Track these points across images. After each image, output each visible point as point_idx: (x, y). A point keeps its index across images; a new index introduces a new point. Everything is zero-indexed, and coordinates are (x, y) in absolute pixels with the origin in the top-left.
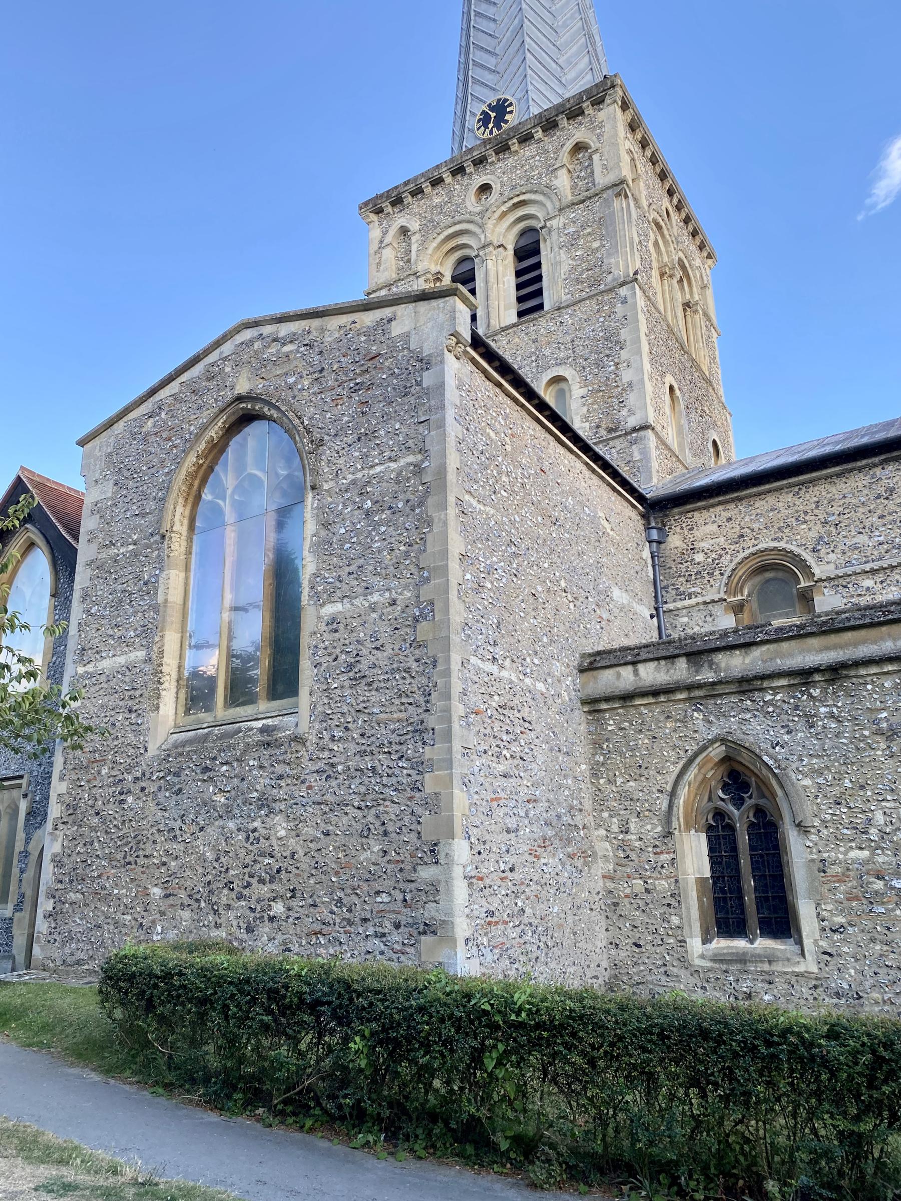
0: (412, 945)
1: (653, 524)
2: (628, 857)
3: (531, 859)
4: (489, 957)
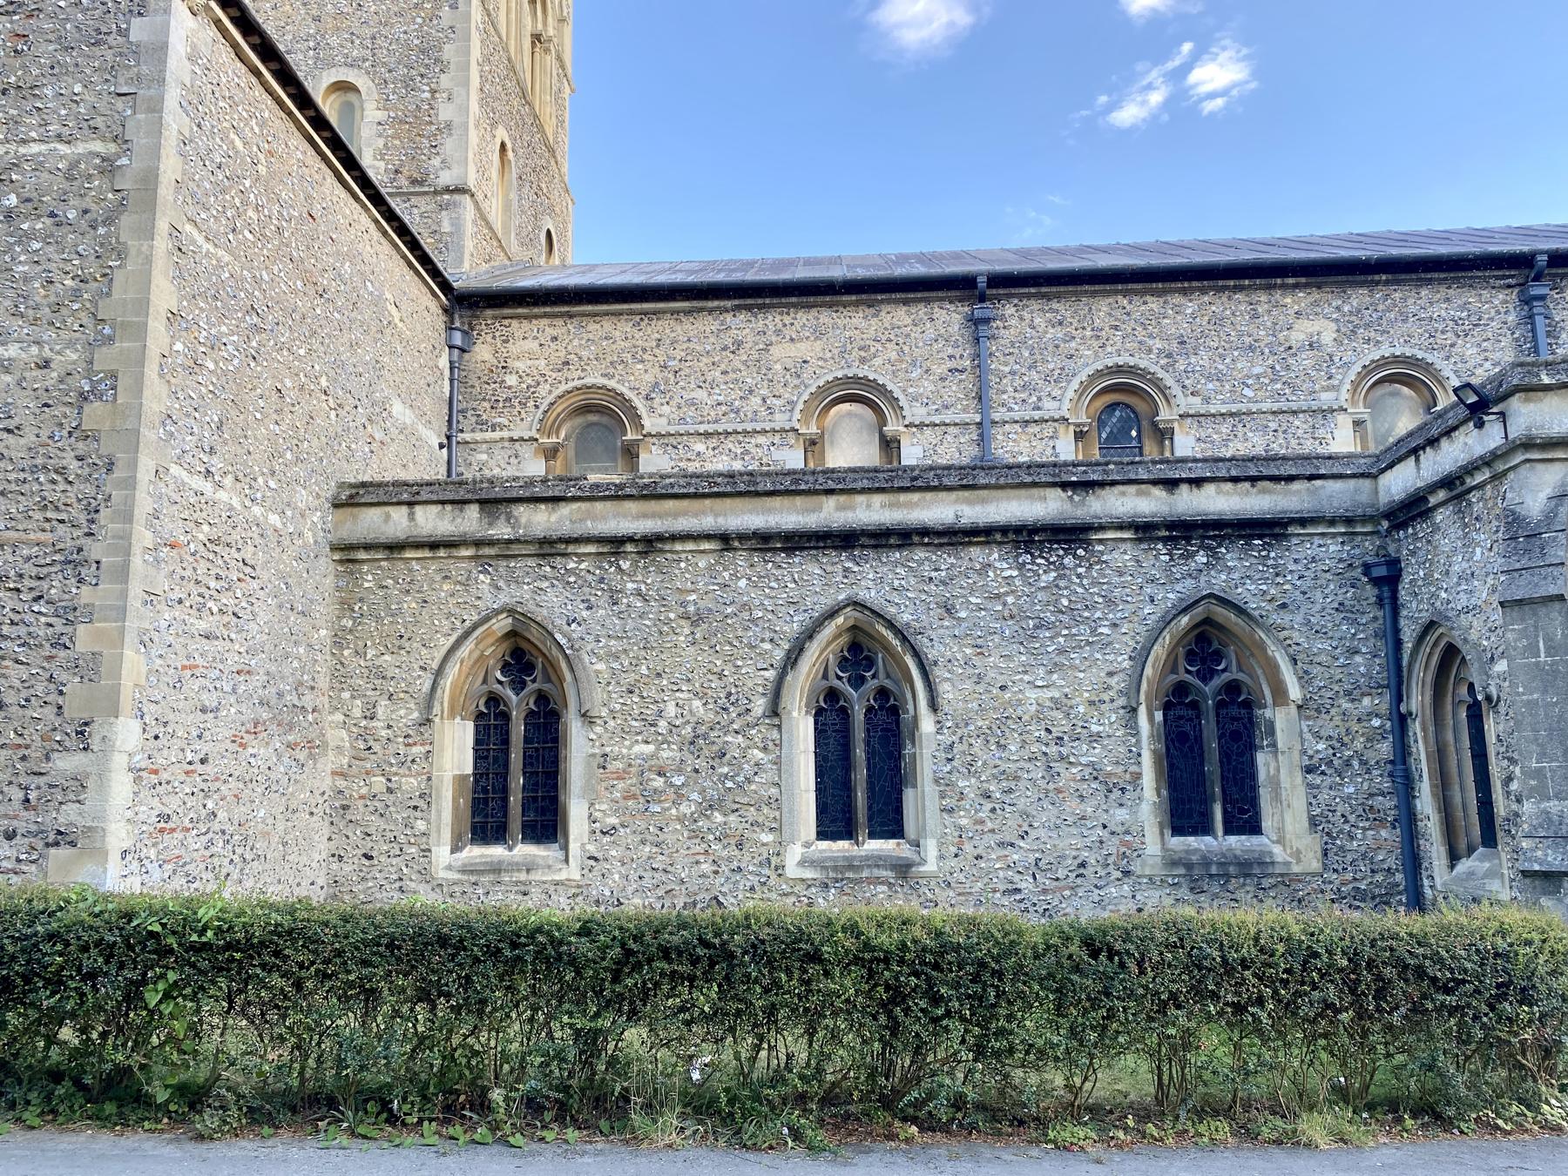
1: (457, 324)
3: (235, 747)
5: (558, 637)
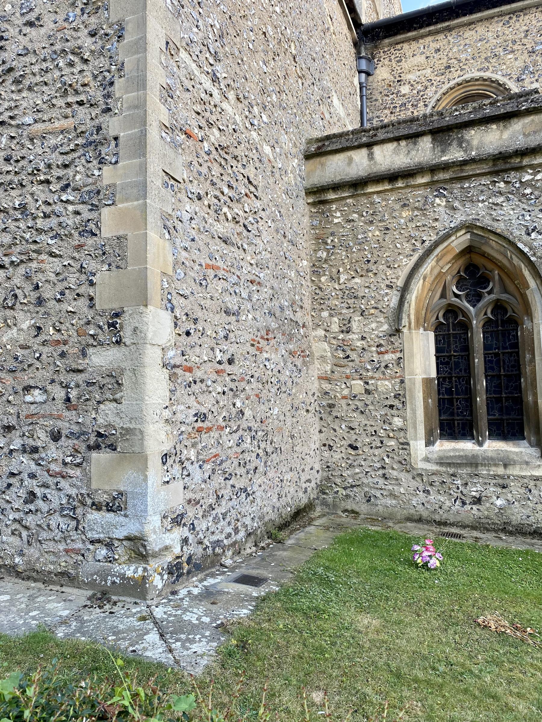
0: (78, 465)
1: (363, 54)
2: (348, 357)
3: (253, 351)
4: (197, 475)
5: (521, 245)
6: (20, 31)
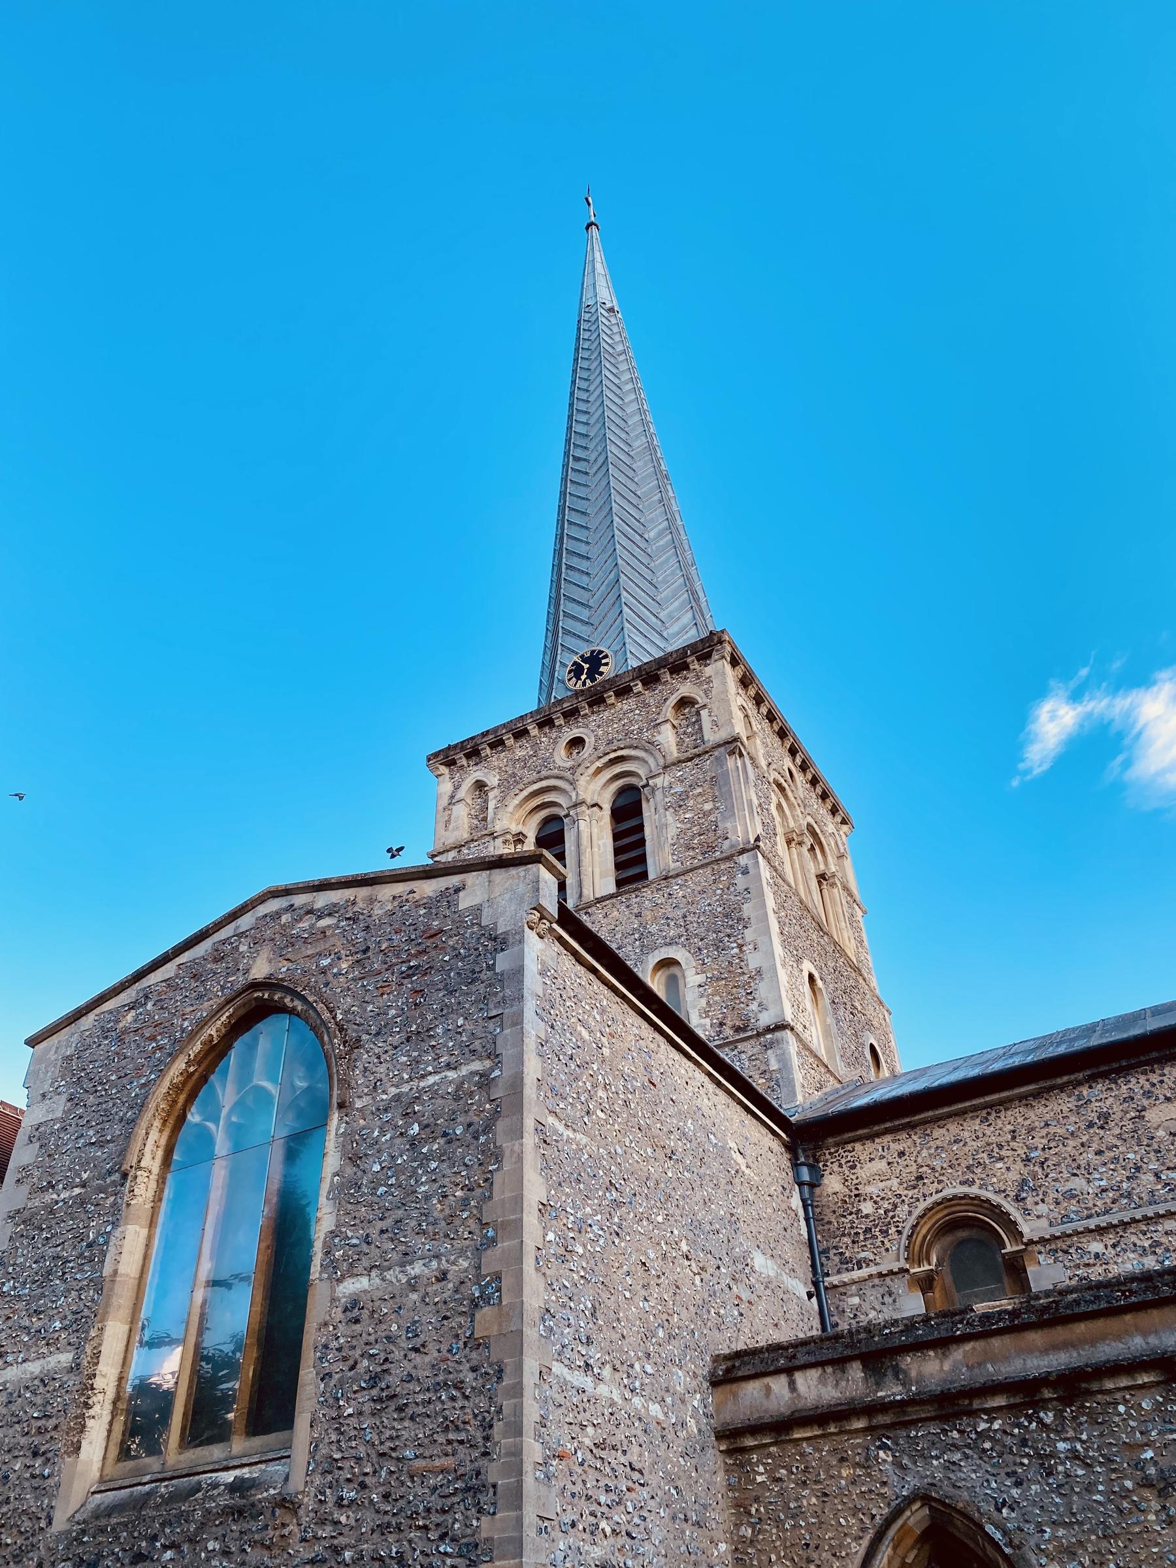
6: (405, 1356)
